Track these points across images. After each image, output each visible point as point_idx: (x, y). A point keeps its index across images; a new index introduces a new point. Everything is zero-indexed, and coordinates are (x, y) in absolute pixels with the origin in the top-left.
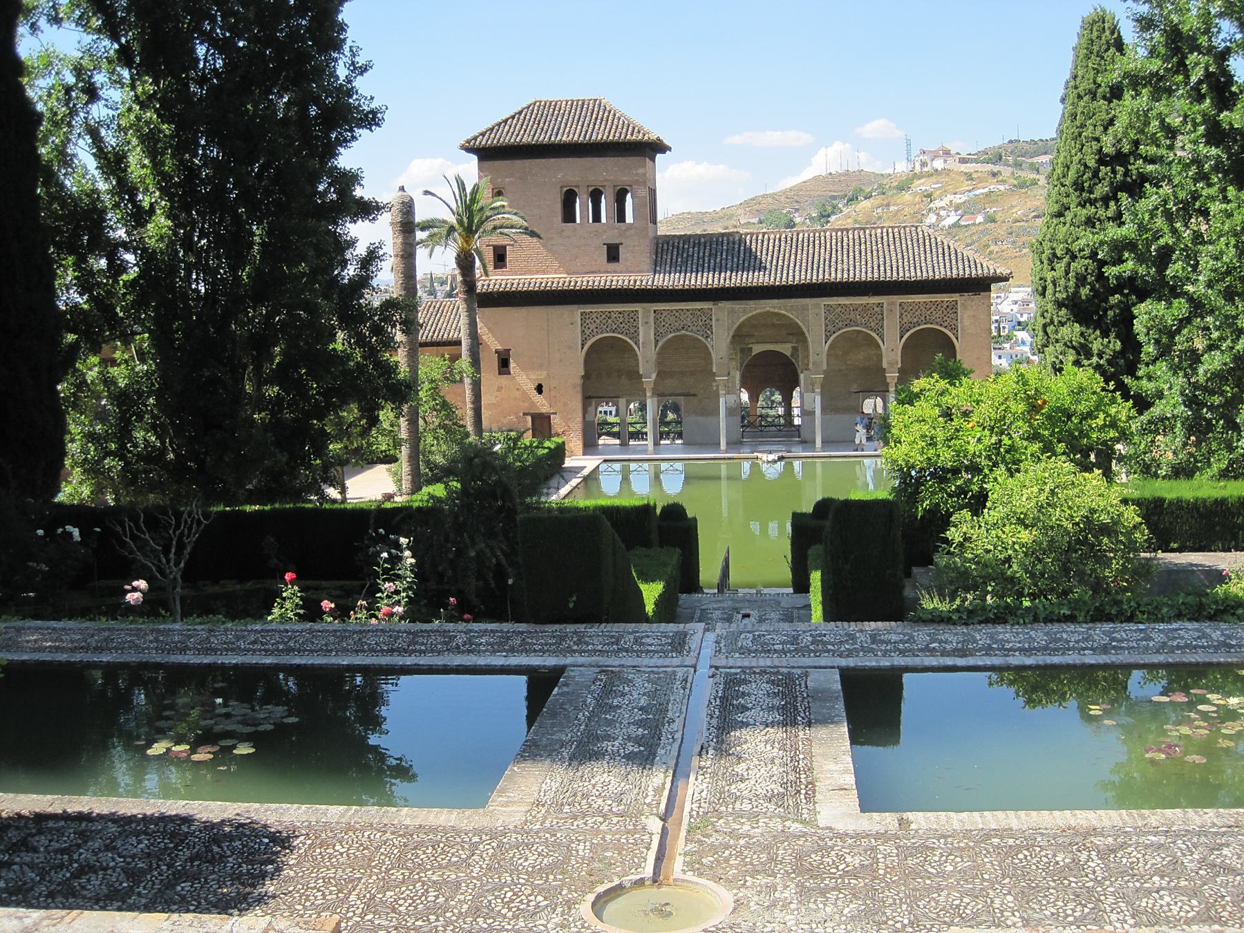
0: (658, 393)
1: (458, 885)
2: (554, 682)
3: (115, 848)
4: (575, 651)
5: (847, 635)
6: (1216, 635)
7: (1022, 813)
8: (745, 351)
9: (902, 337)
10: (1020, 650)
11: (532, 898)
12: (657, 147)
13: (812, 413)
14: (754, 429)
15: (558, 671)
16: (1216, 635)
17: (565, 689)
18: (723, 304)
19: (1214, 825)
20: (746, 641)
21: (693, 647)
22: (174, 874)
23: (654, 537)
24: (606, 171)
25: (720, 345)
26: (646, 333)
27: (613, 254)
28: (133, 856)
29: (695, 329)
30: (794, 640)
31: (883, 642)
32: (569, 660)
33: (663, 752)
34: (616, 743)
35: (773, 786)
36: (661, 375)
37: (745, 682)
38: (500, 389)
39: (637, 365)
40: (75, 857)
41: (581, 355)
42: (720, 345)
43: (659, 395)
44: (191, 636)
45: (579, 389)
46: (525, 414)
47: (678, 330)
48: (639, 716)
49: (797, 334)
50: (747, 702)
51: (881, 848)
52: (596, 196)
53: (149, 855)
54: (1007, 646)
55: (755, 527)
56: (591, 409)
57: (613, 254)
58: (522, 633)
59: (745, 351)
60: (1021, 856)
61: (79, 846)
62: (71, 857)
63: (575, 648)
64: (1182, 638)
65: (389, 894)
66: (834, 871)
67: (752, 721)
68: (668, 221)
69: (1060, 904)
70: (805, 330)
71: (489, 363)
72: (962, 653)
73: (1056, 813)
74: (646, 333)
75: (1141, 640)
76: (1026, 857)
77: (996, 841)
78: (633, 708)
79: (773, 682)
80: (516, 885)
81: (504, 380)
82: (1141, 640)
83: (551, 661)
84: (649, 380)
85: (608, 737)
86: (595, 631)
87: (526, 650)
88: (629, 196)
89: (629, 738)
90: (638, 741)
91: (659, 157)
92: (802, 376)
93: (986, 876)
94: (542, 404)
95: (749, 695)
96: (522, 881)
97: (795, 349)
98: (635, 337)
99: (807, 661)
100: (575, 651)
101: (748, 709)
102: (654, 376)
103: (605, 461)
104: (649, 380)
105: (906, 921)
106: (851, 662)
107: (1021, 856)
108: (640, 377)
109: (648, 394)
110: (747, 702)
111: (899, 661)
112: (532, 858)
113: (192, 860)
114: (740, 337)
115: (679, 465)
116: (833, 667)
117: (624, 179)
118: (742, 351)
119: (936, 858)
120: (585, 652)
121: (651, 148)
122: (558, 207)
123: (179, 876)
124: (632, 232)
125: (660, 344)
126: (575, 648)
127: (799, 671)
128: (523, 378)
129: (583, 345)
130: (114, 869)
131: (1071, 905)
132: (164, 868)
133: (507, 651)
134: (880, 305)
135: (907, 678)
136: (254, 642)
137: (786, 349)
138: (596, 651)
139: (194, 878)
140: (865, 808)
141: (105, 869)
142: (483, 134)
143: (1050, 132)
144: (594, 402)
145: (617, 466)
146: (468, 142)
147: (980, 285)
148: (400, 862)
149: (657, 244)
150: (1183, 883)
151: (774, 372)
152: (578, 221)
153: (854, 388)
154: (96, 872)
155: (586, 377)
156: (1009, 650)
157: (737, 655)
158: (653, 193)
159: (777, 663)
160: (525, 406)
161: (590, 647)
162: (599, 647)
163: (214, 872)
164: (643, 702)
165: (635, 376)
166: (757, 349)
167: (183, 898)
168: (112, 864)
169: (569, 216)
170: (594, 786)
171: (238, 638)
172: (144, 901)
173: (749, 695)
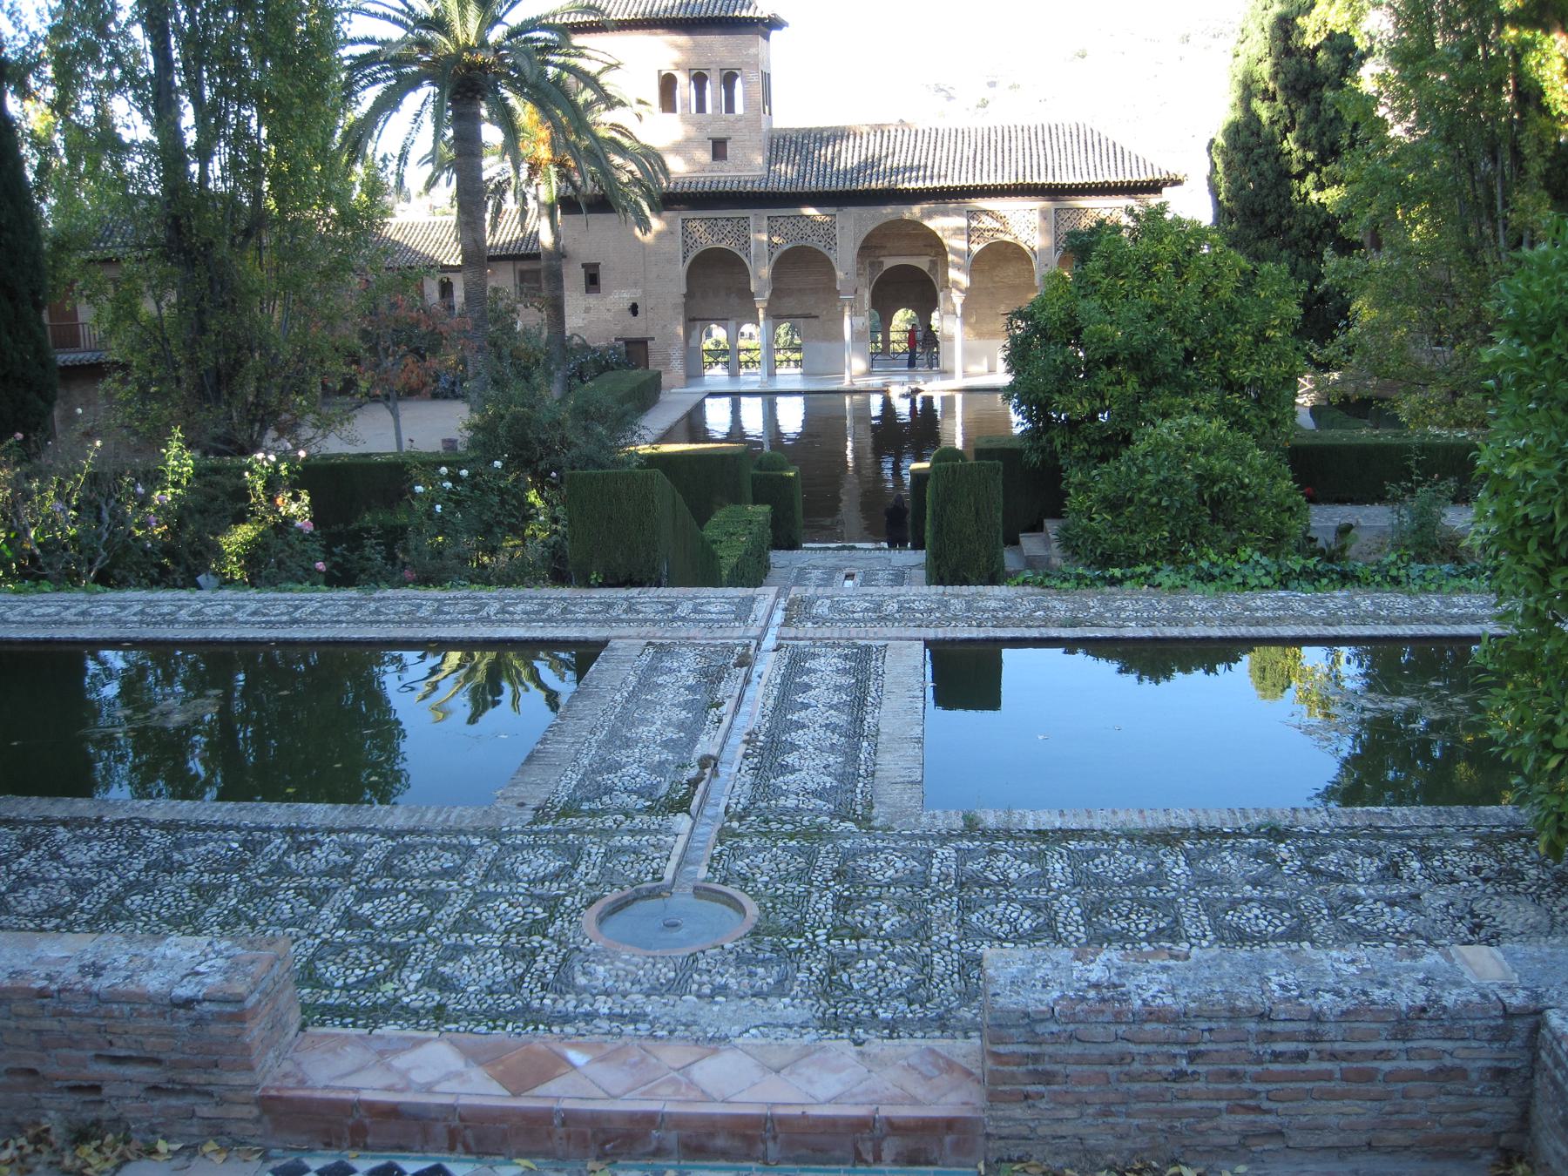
1: (447, 895)
3: (61, 856)
4: (622, 621)
6: (1366, 604)
8: (875, 265)
15: (603, 644)
16: (1366, 604)
19: (1325, 825)
21: (760, 615)
22: (124, 885)
23: (749, 493)
24: (718, 47)
25: (844, 259)
28: (81, 866)
30: (878, 607)
31: (980, 609)
32: (614, 633)
35: (826, 778)
37: (814, 656)
38: (587, 310)
40: (15, 867)
41: (681, 269)
42: (844, 259)
44: (180, 608)
45: (681, 310)
52: (699, 79)
53: (99, 864)
56: (696, 333)
57: (719, 148)
58: (564, 599)
59: (875, 265)
61: (20, 856)
62: (8, 867)
65: (367, 905)
67: (813, 702)
69: (1133, 916)
71: (574, 278)
72: (1074, 623)
81: (592, 300)
83: (591, 633)
85: (643, 721)
86: (648, 597)
87: (565, 617)
88: (738, 82)
90: (681, 726)
91: (774, 34)
94: (637, 328)
95: (815, 671)
97: (933, 264)
99: (891, 631)
100: (622, 621)
106: (941, 633)
107: (1097, 861)
108: (752, 295)
111: (82, 633)
113: (147, 868)
114: (869, 248)
117: (730, 61)
118: (872, 265)
123: (130, 887)
124: (741, 124)
125: (692, 256)
128: (617, 298)
130: (56, 880)
131: (1145, 919)
132: (114, 879)
133: (543, 621)
135: (1007, 654)
136: (254, 614)
137: (922, 263)
139: (147, 889)
141: (46, 881)
144: (698, 324)
148: (387, 867)
149: (772, 139)
154: (35, 885)
155: (689, 295)
158: (766, 78)
159: (854, 633)
160: (617, 330)
163: (170, 883)
164: (691, 681)
165: (747, 295)
166: (889, 263)
167: (132, 913)
168: (55, 875)
171: (237, 608)
172: (86, 917)
173: (815, 671)
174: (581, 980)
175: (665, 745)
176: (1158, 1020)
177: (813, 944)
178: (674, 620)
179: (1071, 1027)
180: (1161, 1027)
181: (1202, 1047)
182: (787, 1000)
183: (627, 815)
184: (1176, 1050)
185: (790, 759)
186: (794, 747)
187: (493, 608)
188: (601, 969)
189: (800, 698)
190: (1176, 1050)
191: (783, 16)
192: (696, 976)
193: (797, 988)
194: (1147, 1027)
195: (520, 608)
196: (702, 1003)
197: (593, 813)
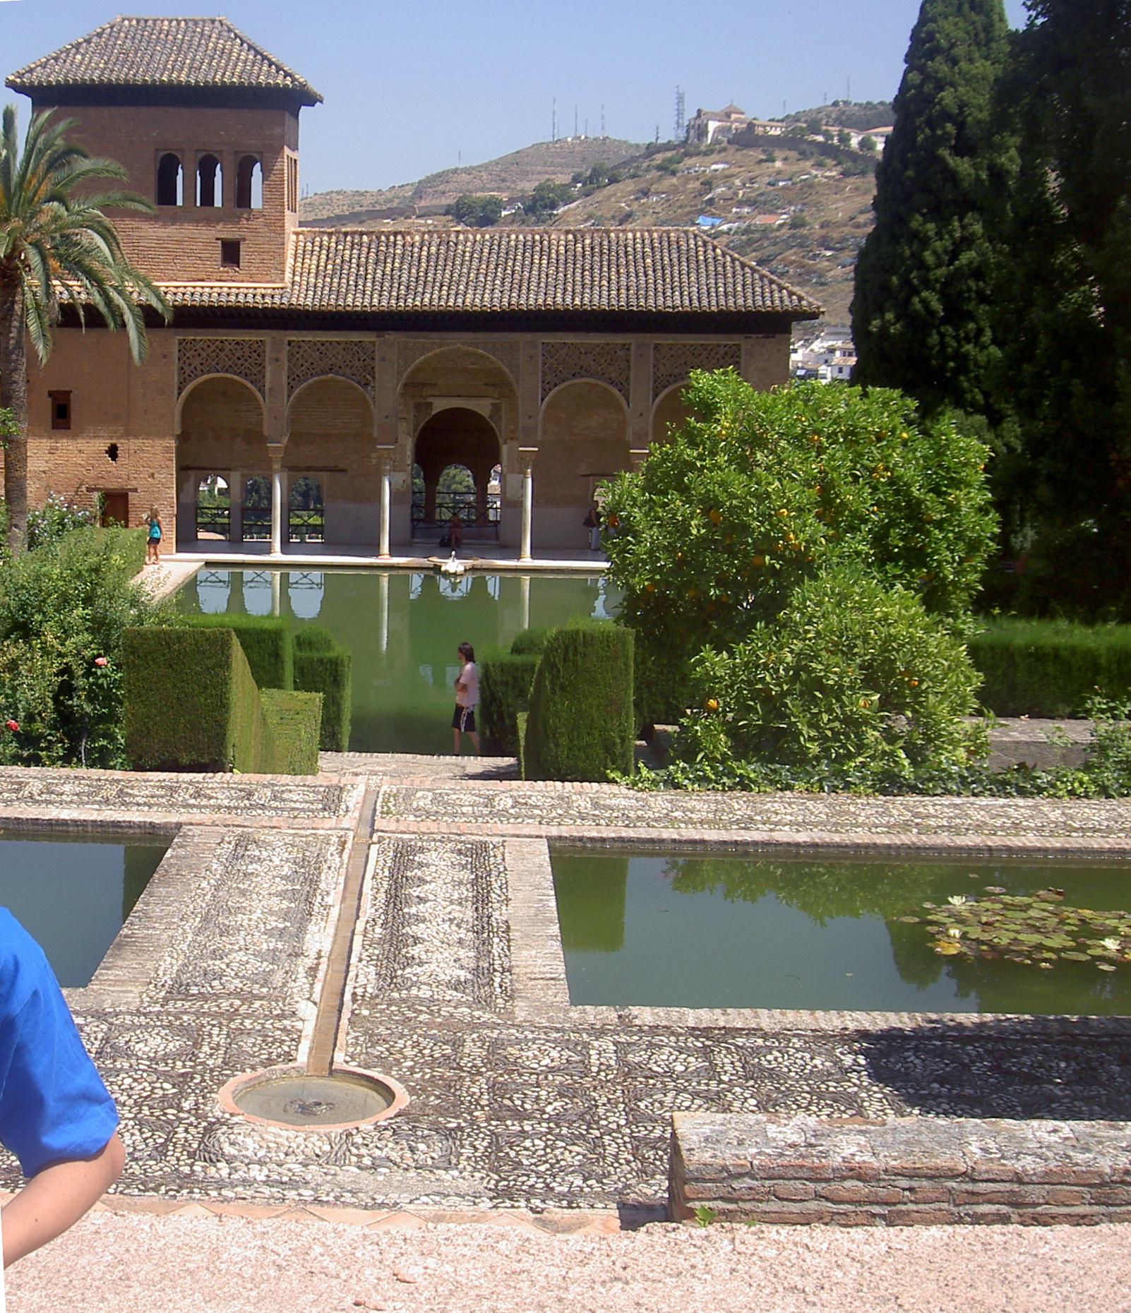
0: (291, 468)
2: (168, 840)
5: (561, 798)
6: (1055, 815)
7: (776, 1012)
8: (421, 407)
9: (546, 392)
10: (791, 824)
11: (158, 1085)
12: (311, 99)
13: (520, 504)
14: (429, 528)
16: (1055, 815)
17: (182, 852)
18: (391, 336)
20: (423, 800)
23: (289, 673)
24: (223, 129)
26: (275, 375)
27: (231, 252)
29: (348, 371)
33: (315, 929)
34: (254, 917)
36: (297, 438)
37: (422, 850)
39: (260, 423)
42: (387, 394)
43: (291, 469)
46: (89, 490)
47: (323, 373)
48: (281, 886)
49: (500, 385)
50: (426, 873)
51: (596, 1044)
54: (774, 818)
55: (427, 672)
56: (189, 486)
57: (231, 252)
58: (118, 781)
59: (421, 407)
60: (769, 1057)
63: (192, 801)
64: (1009, 817)
66: (536, 1066)
68: (348, 221)
70: (512, 379)
73: (819, 1014)
74: (275, 375)
75: (956, 817)
76: (776, 1059)
77: (740, 1041)
78: (274, 877)
79: (460, 852)
80: (136, 1070)
82: (956, 817)
84: (277, 447)
88: (257, 167)
89: (271, 913)
92: (504, 449)
93: (725, 1078)
95: (427, 865)
96: (142, 1067)
97: (496, 407)
98: (258, 381)
101: (425, 882)
102: (285, 440)
103: (208, 564)
104: (277, 447)
105: (623, 1122)
109: (277, 466)
110: (426, 873)
112: (152, 1042)
114: (415, 387)
115: (316, 575)
116: (541, 837)
118: (418, 407)
119: (665, 1057)
120: (205, 807)
121: (300, 97)
122: (151, 180)
126: (192, 801)
127: (496, 840)
129: (180, 390)
133: (99, 803)
134: (626, 347)
137: (482, 407)
138: (219, 807)
140: (574, 1001)
142: (44, 66)
143: (889, 93)
144: (192, 474)
145: (223, 574)
146: (21, 76)
147: (775, 326)
150: (969, 1091)
151: (453, 441)
152: (180, 202)
153: (583, 469)
156: (776, 824)
157: (412, 818)
161: (212, 802)
162: (226, 802)
164: (286, 871)
165: (255, 438)
166: (440, 405)
169: (166, 195)
170: (228, 966)
173: (427, 865)
174: (228, 1149)
175: (269, 933)
176: (859, 1178)
177: (473, 1122)
178: (252, 807)
179: (767, 1183)
180: (861, 1184)
181: (904, 1208)
182: (456, 1173)
183: (244, 1001)
184: (876, 1209)
185: (416, 951)
186: (416, 940)
187: (35, 786)
188: (249, 1141)
189: (415, 892)
190: (876, 1209)
191: (315, 87)
192: (354, 1151)
193: (463, 1163)
194: (848, 1184)
195: (67, 788)
196: (364, 1174)
197: (204, 997)
